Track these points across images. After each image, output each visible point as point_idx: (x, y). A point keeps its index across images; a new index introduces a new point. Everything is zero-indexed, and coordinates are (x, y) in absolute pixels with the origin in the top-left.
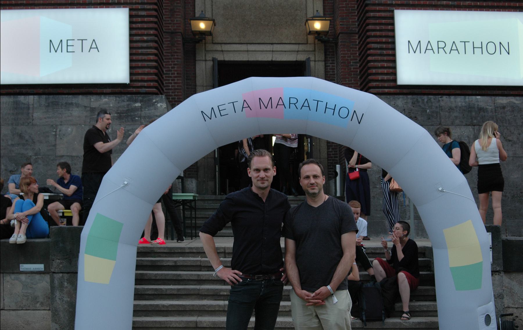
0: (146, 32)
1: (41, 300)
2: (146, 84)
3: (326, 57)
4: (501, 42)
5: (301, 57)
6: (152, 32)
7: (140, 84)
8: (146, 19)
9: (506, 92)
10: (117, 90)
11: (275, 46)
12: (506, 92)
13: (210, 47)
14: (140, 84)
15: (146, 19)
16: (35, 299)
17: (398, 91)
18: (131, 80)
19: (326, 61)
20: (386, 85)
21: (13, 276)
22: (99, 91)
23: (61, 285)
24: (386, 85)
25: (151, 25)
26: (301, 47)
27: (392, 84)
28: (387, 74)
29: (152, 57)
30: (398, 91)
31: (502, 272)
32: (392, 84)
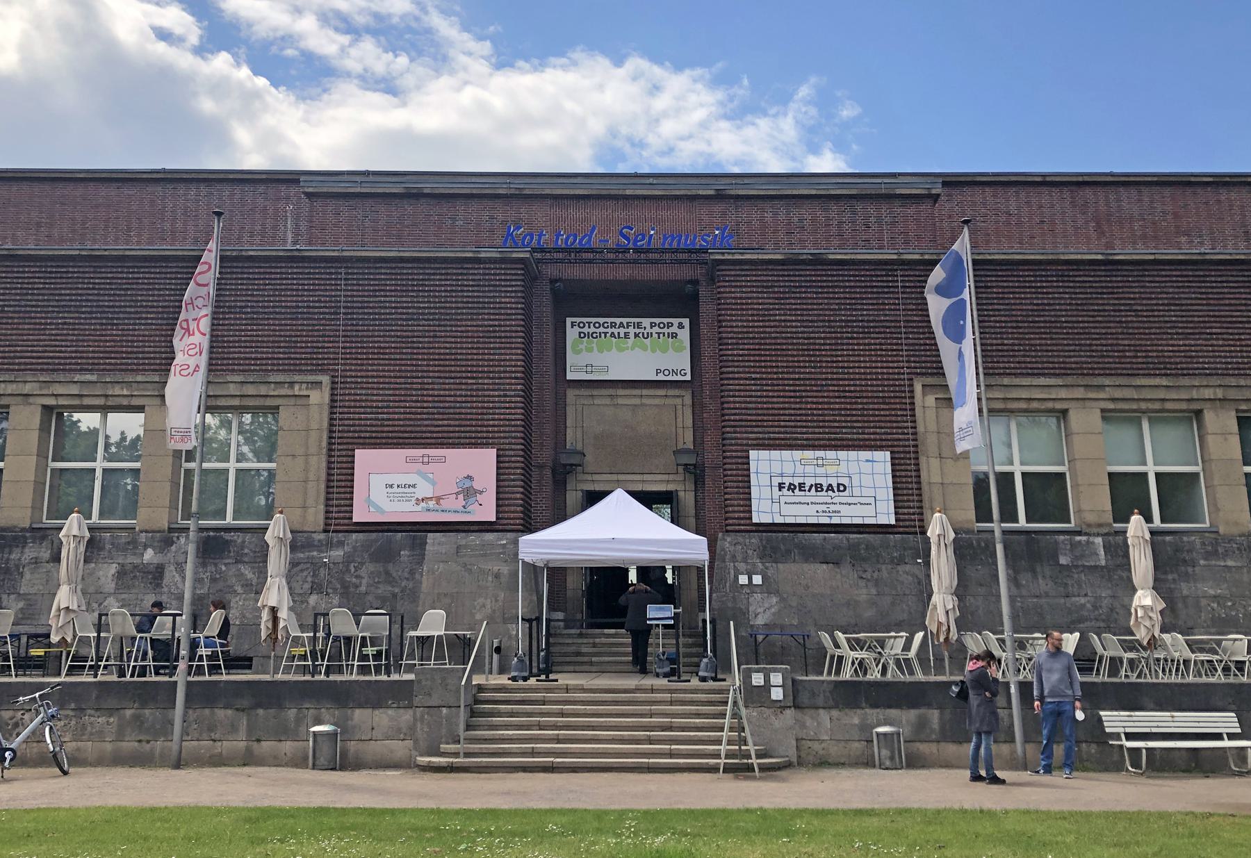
0: (512, 471)
1: (404, 730)
2: (512, 522)
3: (696, 487)
4: (66, 777)
5: (671, 487)
6: (519, 351)
7: (506, 522)
8: (513, 459)
9: (862, 530)
10: (483, 527)
11: (645, 476)
12: (862, 530)
13: (580, 477)
14: (506, 522)
15: (513, 459)
16: (399, 730)
17: (754, 528)
18: (497, 518)
19: (696, 491)
20: (742, 522)
21: (381, 710)
22: (466, 528)
23: (422, 716)
24: (742, 522)
25: (519, 345)
26: (671, 477)
27: (748, 522)
28: (743, 512)
29: (519, 509)
30: (754, 528)
31: (316, 543)
32: (748, 522)
